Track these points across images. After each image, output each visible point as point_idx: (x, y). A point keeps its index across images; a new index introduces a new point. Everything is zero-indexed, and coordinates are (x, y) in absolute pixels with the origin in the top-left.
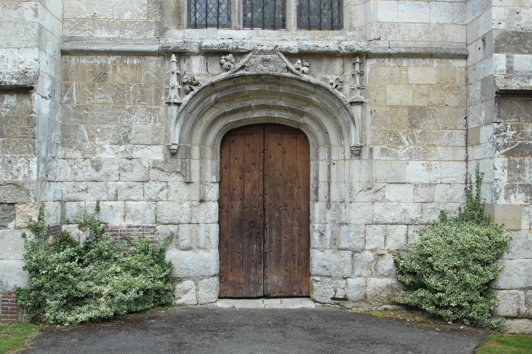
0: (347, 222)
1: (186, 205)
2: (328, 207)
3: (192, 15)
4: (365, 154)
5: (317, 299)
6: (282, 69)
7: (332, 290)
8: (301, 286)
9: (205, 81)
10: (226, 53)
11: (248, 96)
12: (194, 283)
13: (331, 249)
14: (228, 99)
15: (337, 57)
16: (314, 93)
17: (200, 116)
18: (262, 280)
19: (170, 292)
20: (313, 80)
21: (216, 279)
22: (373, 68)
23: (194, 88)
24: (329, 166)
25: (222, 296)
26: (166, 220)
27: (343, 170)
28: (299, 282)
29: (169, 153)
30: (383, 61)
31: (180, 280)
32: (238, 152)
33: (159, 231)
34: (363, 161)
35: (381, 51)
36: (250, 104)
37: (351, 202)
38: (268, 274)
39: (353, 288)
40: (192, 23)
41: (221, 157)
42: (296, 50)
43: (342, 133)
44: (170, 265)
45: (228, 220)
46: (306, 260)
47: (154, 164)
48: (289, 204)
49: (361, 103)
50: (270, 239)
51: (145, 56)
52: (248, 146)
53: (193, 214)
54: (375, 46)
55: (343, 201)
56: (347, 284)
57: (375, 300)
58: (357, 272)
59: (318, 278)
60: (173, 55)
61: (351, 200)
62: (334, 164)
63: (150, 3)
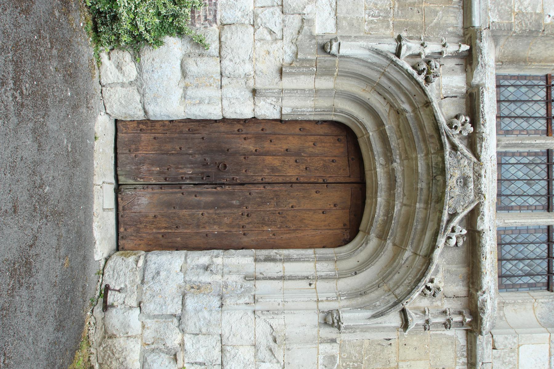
0: (224, 307)
1: (248, 68)
2: (247, 278)
3: (512, 82)
4: (328, 332)
5: (111, 263)
6: (453, 206)
7: (123, 286)
8: (132, 238)
9: (432, 91)
10: (474, 122)
11: (407, 158)
12: (132, 80)
13: (185, 282)
14: (402, 129)
15: (469, 287)
16: (415, 254)
17: (378, 89)
18: (142, 181)
19: (115, 44)
20: (437, 253)
21: (140, 115)
22: (453, 341)
23: (423, 76)
24: (308, 278)
25: (119, 125)
26: (226, 38)
27: (302, 299)
28: (131, 234)
29: (325, 41)
30: (463, 355)
31: (136, 57)
32: (324, 147)
33: (209, 28)
34: (316, 329)
35: (479, 352)
36: (395, 162)
37: (254, 312)
38: (150, 190)
39: (124, 319)
40: (501, 81)
41: (317, 122)
42: (480, 226)
43: (357, 297)
44: (158, 42)
45: (227, 133)
46: (170, 245)
47: (308, 20)
48: (250, 220)
49: (405, 325)
50: (201, 193)
51: (463, 8)
52: (333, 161)
53: (235, 80)
54: (484, 343)
55: (255, 300)
56: (131, 308)
57: (106, 351)
58: (149, 323)
59: (141, 263)
60: (468, 47)
61: (259, 313)
62: (310, 284)
63: (537, 17)
